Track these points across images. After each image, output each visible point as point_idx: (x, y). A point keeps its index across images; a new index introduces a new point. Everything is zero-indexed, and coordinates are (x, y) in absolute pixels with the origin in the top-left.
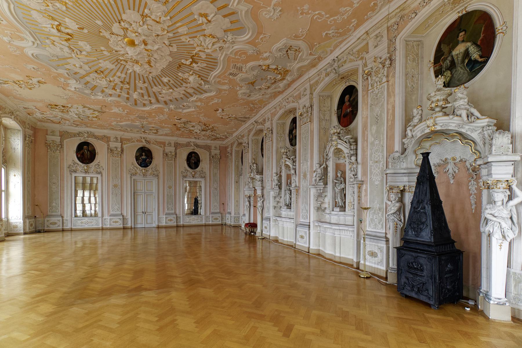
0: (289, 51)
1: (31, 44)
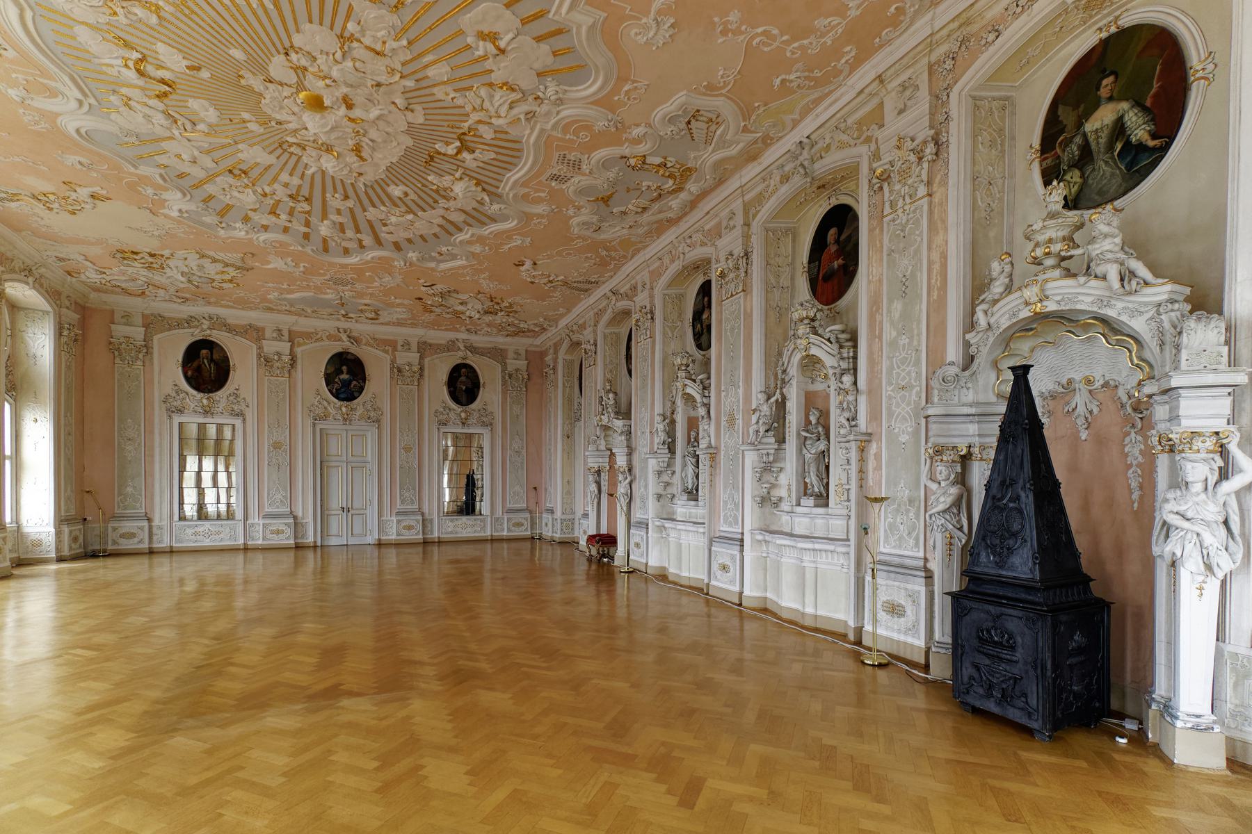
0: (693, 121)
1: (73, 105)
